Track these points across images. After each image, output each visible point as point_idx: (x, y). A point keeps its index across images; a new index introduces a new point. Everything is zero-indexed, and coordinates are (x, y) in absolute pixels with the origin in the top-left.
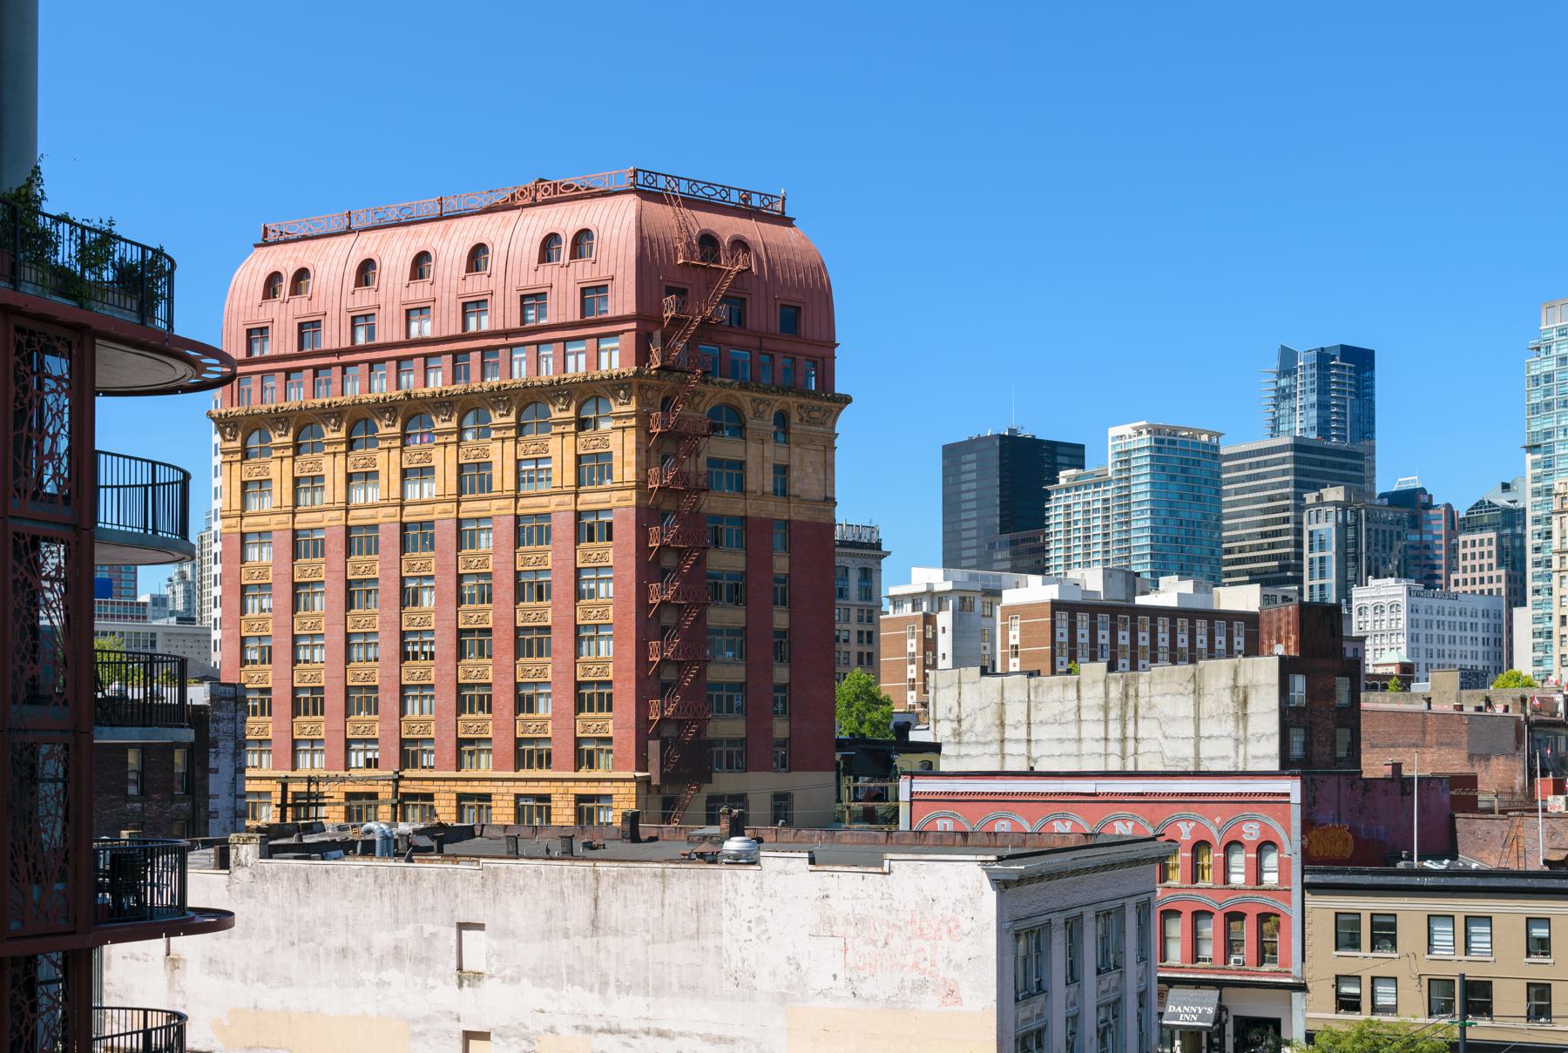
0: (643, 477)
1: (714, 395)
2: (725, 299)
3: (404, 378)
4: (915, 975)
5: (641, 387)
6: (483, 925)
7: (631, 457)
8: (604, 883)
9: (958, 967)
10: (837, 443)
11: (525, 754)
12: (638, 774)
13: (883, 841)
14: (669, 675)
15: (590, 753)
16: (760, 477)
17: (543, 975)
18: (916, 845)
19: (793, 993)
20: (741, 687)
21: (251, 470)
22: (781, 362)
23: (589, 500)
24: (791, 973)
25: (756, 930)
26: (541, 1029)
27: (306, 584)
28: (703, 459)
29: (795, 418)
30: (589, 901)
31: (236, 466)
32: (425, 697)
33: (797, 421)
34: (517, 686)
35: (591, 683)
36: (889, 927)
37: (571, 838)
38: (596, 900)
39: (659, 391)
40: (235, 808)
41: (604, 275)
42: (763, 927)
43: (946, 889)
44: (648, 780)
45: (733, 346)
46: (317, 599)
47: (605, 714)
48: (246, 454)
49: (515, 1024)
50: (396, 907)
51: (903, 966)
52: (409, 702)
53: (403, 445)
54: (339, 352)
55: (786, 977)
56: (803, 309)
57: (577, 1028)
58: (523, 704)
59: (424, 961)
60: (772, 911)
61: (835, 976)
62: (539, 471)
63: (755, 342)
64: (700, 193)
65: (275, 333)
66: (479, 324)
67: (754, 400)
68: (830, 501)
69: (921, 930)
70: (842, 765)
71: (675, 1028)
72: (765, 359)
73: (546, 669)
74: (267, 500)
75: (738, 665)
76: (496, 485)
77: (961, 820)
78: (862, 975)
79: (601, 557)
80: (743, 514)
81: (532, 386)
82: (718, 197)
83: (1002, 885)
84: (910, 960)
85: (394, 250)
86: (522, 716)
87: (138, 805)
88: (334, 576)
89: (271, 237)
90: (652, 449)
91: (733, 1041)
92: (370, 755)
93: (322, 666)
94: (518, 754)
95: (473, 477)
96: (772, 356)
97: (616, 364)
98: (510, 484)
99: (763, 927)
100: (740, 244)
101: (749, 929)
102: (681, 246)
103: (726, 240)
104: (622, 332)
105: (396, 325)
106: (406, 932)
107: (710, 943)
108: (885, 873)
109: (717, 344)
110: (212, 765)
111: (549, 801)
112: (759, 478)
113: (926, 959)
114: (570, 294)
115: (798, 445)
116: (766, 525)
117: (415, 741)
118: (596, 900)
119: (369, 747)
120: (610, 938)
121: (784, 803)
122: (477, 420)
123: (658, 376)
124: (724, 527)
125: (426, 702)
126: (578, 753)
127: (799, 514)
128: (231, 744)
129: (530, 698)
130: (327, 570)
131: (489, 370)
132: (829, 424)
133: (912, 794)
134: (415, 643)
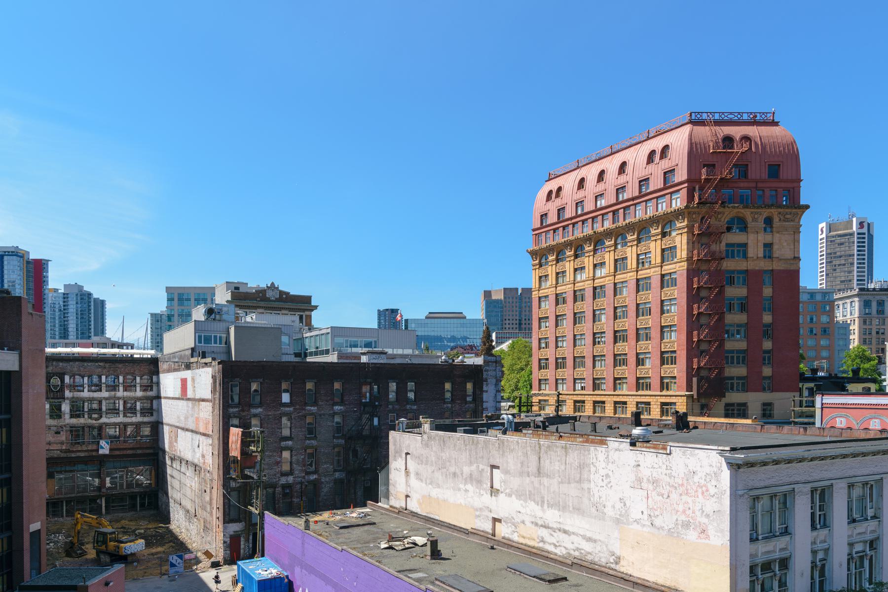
0: (690, 255)
1: (729, 213)
2: (735, 165)
3: (595, 226)
4: (683, 518)
5: (689, 213)
6: (499, 467)
7: (685, 247)
8: (543, 448)
9: (708, 516)
10: (801, 229)
11: (641, 384)
12: (687, 393)
13: (759, 431)
14: (704, 347)
15: (667, 383)
16: (756, 250)
17: (520, 495)
18: (777, 433)
19: (622, 519)
20: (744, 351)
21: (542, 272)
22: (768, 192)
23: (667, 269)
24: (622, 508)
25: (606, 481)
26: (519, 521)
27: (560, 315)
28: (723, 244)
29: (776, 220)
30: (537, 458)
31: (537, 270)
32: (602, 360)
33: (778, 220)
34: (637, 354)
35: (667, 352)
36: (670, 486)
37: (595, 424)
38: (539, 458)
39: (699, 214)
40: (496, 407)
41: (674, 164)
42: (608, 480)
43: (701, 466)
44: (692, 396)
45: (741, 188)
46: (565, 321)
47: (673, 366)
48: (541, 265)
49: (510, 517)
50: (470, 455)
51: (677, 511)
52: (597, 362)
53: (595, 253)
54: (571, 219)
55: (619, 509)
56: (781, 165)
57: (532, 523)
58: (640, 362)
59: (479, 482)
60: (613, 471)
61: (642, 512)
62: (646, 258)
63: (753, 185)
64: (726, 118)
65: (550, 215)
66: (623, 197)
67: (752, 213)
68: (797, 259)
69: (687, 490)
70: (815, 389)
71: (571, 529)
72: (760, 193)
73: (651, 347)
74: (548, 282)
75: (743, 341)
76: (629, 267)
77: (851, 419)
78: (657, 513)
79: (672, 294)
80: (746, 269)
81: (642, 220)
82: (736, 118)
83: (735, 467)
84: (681, 508)
85: (591, 173)
86: (639, 367)
87: (450, 405)
88: (570, 311)
89: (553, 176)
90: (698, 239)
91: (595, 541)
92: (583, 385)
93: (566, 349)
94: (638, 383)
95: (620, 263)
96: (763, 191)
97: (679, 204)
98: (634, 265)
99: (608, 480)
100: (746, 138)
101: (603, 480)
102: (711, 144)
103: (738, 137)
104: (681, 189)
105: (592, 203)
106: (474, 467)
107: (585, 486)
108: (667, 454)
109: (732, 188)
110: (485, 388)
111: (626, 404)
112: (755, 250)
113: (689, 509)
114: (659, 176)
115: (778, 232)
116: (760, 273)
117: (598, 379)
118: (539, 458)
119: (582, 381)
120: (545, 478)
121: (769, 408)
122: (622, 239)
123: (698, 207)
124: (736, 276)
125: (603, 362)
126: (662, 383)
127: (777, 266)
128: (494, 381)
129: (643, 359)
130: (567, 309)
131: (627, 216)
132: (797, 220)
133: (822, 404)
134: (599, 338)
